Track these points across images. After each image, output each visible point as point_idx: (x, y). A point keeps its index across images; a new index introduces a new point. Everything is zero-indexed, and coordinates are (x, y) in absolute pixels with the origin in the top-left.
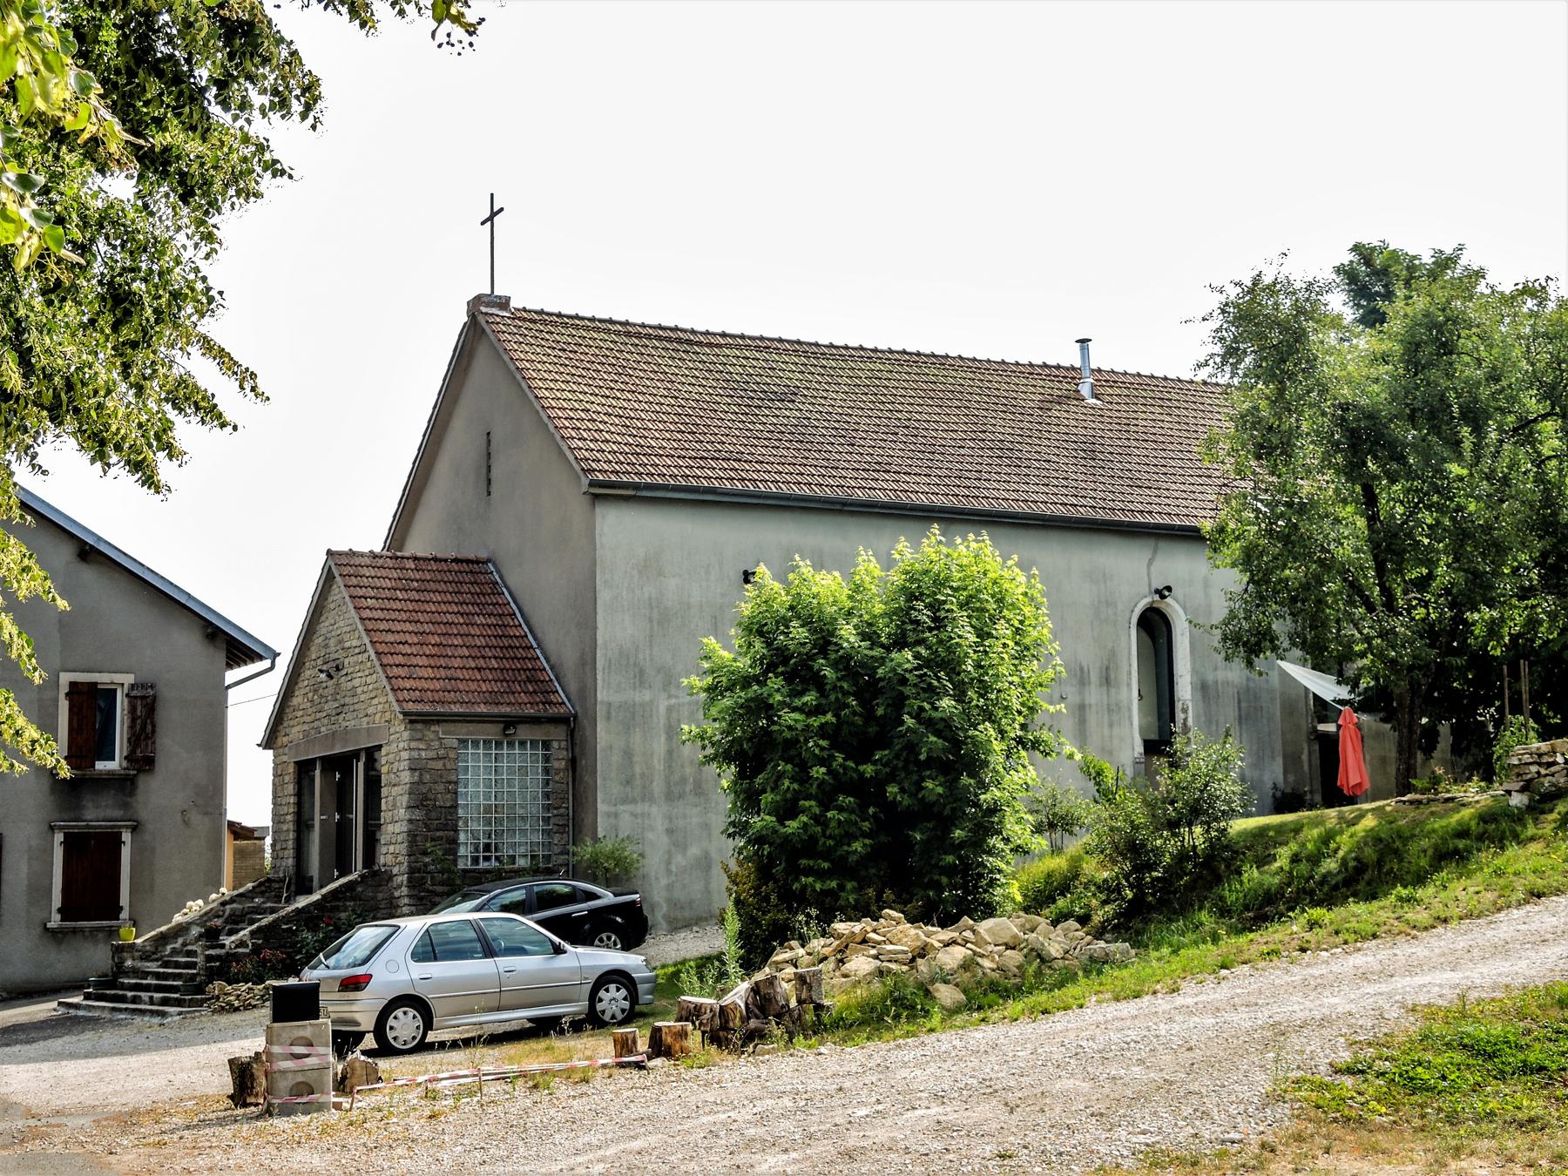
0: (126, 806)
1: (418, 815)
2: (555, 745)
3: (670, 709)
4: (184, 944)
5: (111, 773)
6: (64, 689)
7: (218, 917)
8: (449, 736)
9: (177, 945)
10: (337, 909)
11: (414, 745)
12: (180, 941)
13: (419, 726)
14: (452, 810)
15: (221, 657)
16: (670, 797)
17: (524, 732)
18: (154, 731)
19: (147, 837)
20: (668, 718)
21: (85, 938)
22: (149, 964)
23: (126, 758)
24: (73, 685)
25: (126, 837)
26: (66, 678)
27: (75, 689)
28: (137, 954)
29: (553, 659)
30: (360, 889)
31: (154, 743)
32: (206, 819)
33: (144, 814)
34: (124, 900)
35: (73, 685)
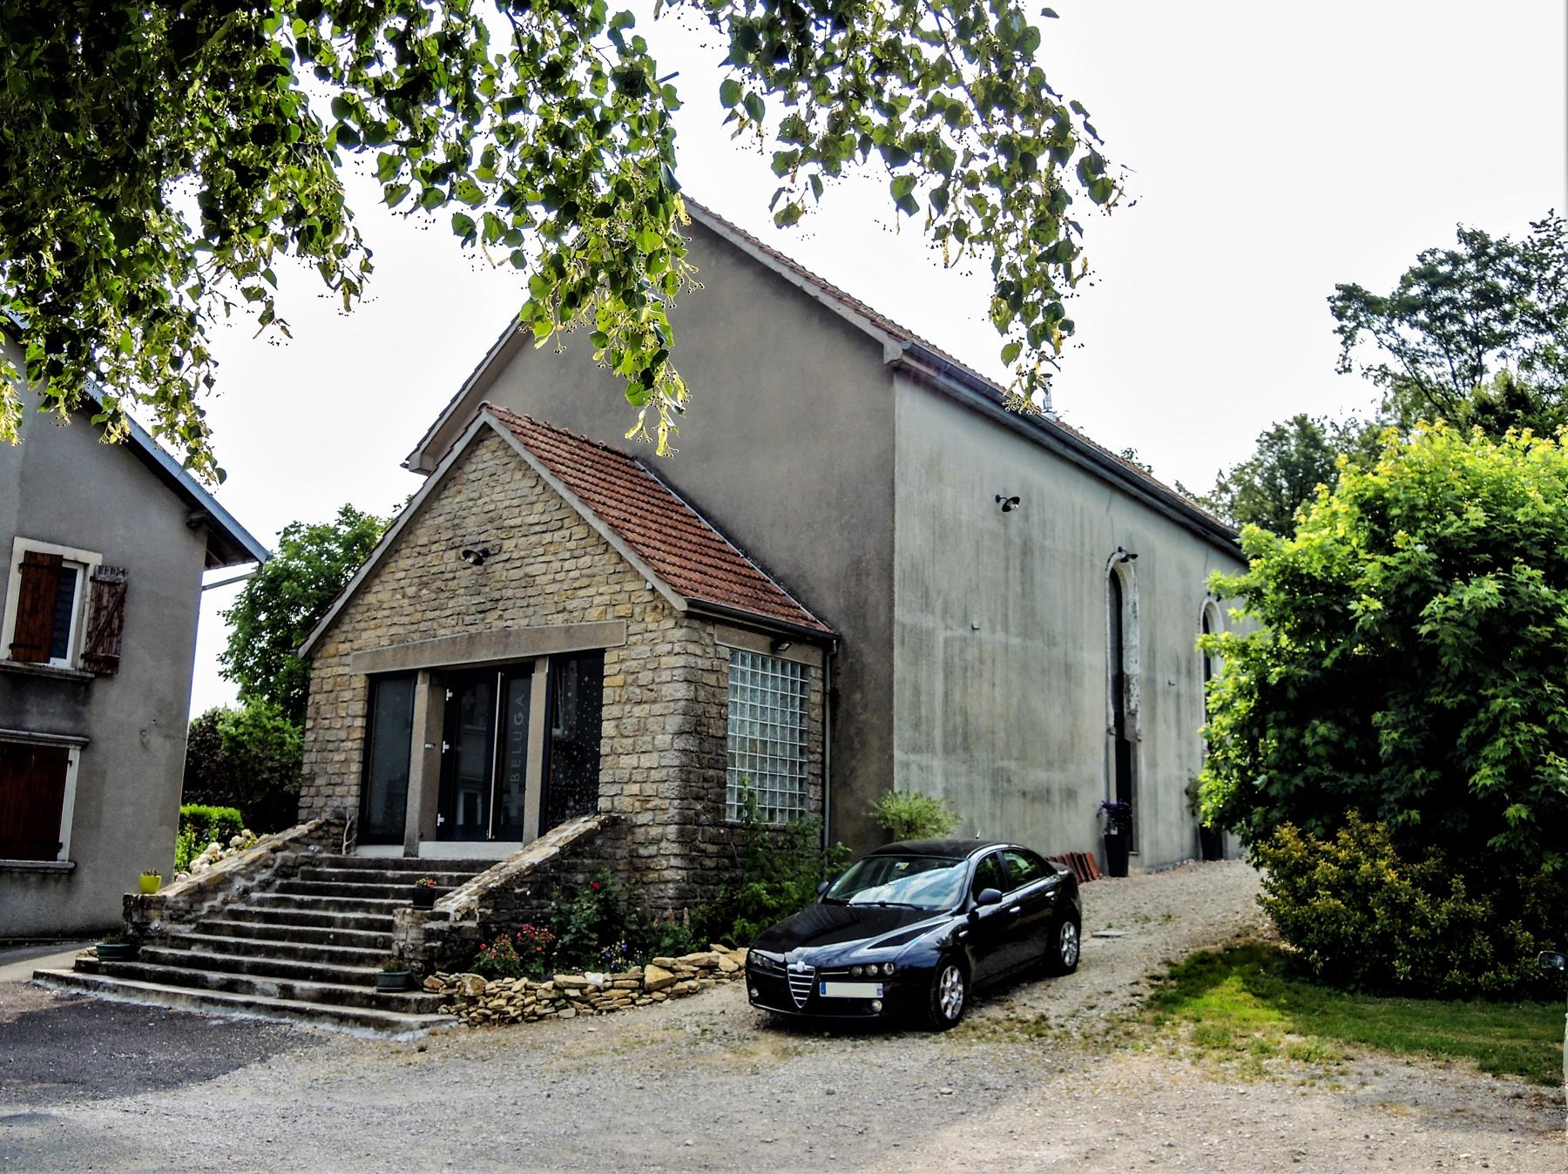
0: (77, 717)
1: (691, 743)
2: (813, 672)
3: (946, 641)
4: (225, 902)
5: (62, 673)
6: (18, 559)
7: (267, 867)
8: (725, 640)
9: (217, 903)
10: (573, 868)
11: (691, 648)
12: (221, 896)
13: (696, 624)
14: (723, 742)
15: (201, 552)
16: (948, 750)
17: (791, 653)
18: (120, 628)
19: (98, 758)
20: (945, 652)
21: (13, 880)
22: (180, 927)
23: (82, 656)
24: (29, 555)
25: (74, 755)
26: (21, 545)
27: (32, 562)
28: (166, 913)
29: (781, 570)
30: (599, 842)
31: (119, 642)
32: (168, 744)
33: (98, 729)
34: (65, 836)
35: (29, 555)
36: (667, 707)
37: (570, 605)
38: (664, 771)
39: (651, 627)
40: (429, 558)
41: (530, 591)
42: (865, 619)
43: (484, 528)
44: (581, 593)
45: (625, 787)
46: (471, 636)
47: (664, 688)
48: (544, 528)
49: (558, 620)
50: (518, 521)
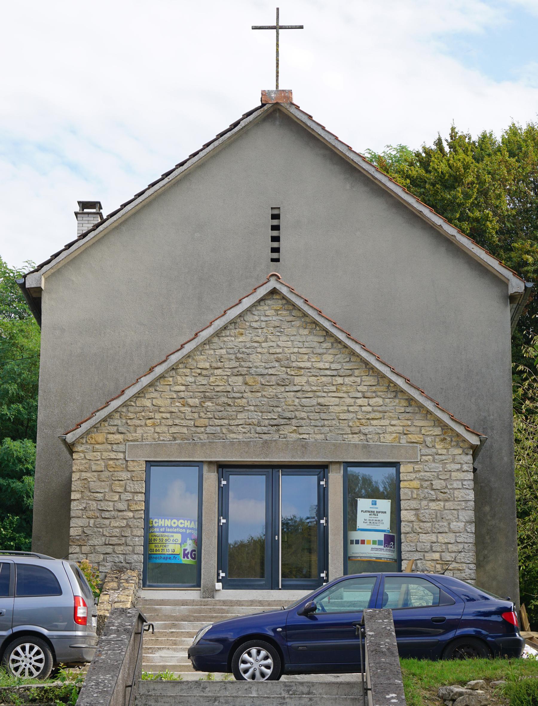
36: (459, 505)
37: (364, 429)
38: (461, 546)
39: (440, 452)
40: (212, 379)
41: (323, 416)
42: (491, 458)
43: (271, 365)
44: (374, 422)
45: (426, 554)
46: (266, 442)
47: (456, 492)
48: (335, 373)
49: (356, 439)
50: (308, 365)
